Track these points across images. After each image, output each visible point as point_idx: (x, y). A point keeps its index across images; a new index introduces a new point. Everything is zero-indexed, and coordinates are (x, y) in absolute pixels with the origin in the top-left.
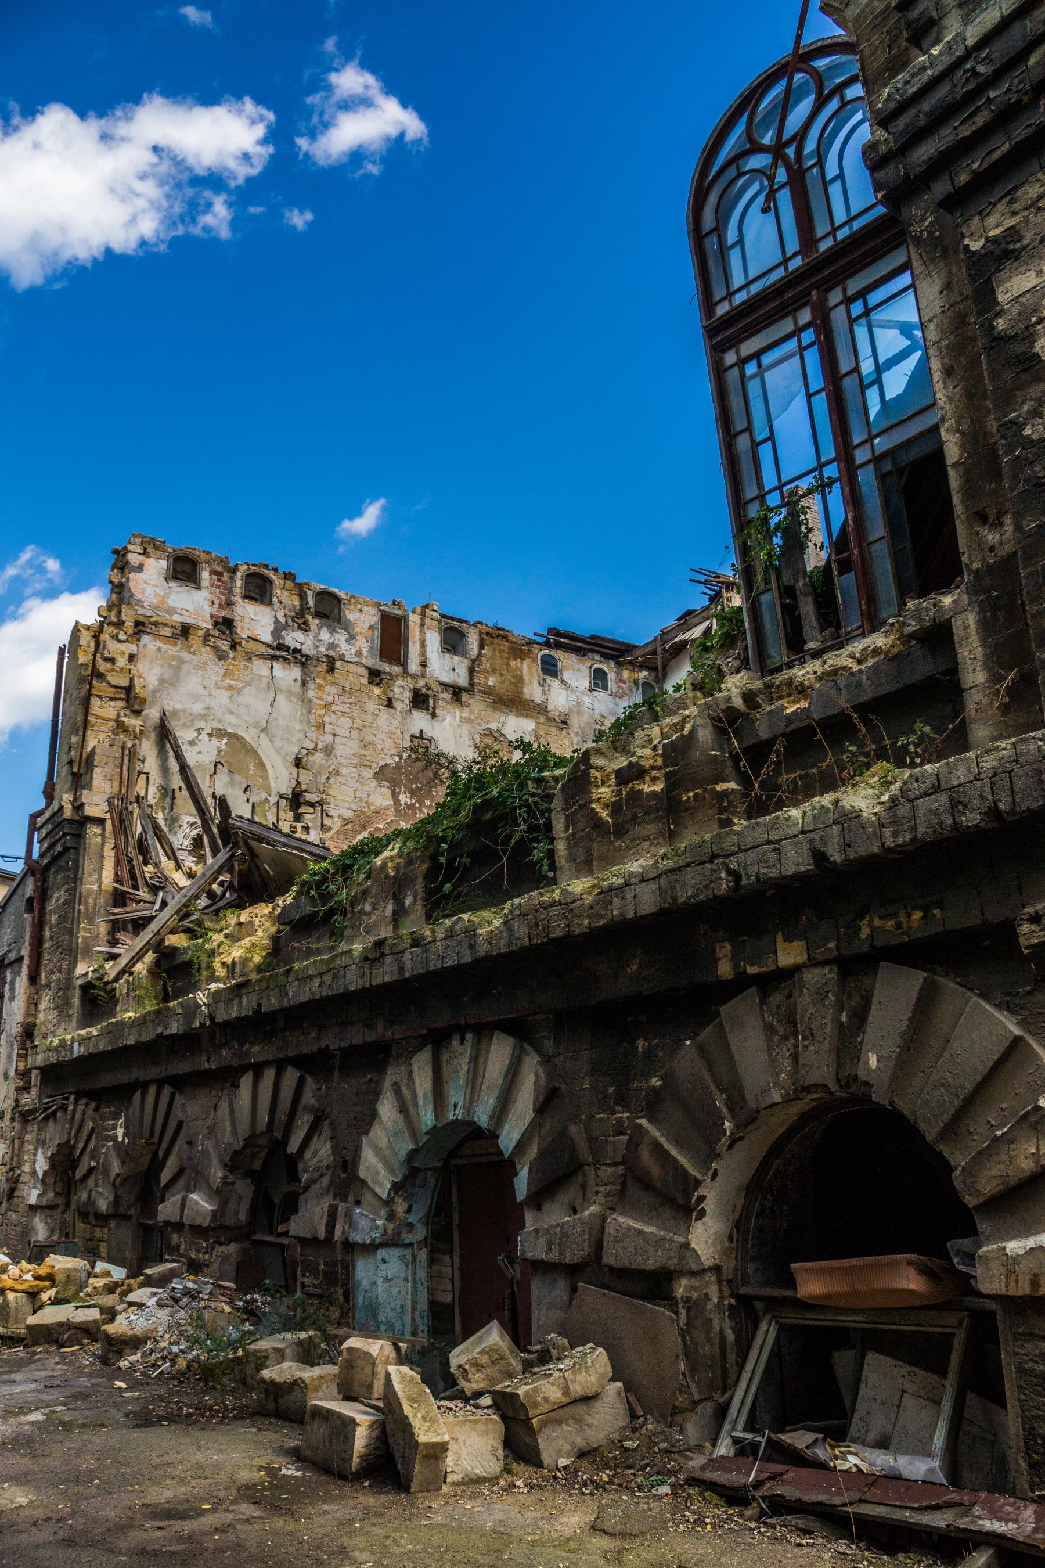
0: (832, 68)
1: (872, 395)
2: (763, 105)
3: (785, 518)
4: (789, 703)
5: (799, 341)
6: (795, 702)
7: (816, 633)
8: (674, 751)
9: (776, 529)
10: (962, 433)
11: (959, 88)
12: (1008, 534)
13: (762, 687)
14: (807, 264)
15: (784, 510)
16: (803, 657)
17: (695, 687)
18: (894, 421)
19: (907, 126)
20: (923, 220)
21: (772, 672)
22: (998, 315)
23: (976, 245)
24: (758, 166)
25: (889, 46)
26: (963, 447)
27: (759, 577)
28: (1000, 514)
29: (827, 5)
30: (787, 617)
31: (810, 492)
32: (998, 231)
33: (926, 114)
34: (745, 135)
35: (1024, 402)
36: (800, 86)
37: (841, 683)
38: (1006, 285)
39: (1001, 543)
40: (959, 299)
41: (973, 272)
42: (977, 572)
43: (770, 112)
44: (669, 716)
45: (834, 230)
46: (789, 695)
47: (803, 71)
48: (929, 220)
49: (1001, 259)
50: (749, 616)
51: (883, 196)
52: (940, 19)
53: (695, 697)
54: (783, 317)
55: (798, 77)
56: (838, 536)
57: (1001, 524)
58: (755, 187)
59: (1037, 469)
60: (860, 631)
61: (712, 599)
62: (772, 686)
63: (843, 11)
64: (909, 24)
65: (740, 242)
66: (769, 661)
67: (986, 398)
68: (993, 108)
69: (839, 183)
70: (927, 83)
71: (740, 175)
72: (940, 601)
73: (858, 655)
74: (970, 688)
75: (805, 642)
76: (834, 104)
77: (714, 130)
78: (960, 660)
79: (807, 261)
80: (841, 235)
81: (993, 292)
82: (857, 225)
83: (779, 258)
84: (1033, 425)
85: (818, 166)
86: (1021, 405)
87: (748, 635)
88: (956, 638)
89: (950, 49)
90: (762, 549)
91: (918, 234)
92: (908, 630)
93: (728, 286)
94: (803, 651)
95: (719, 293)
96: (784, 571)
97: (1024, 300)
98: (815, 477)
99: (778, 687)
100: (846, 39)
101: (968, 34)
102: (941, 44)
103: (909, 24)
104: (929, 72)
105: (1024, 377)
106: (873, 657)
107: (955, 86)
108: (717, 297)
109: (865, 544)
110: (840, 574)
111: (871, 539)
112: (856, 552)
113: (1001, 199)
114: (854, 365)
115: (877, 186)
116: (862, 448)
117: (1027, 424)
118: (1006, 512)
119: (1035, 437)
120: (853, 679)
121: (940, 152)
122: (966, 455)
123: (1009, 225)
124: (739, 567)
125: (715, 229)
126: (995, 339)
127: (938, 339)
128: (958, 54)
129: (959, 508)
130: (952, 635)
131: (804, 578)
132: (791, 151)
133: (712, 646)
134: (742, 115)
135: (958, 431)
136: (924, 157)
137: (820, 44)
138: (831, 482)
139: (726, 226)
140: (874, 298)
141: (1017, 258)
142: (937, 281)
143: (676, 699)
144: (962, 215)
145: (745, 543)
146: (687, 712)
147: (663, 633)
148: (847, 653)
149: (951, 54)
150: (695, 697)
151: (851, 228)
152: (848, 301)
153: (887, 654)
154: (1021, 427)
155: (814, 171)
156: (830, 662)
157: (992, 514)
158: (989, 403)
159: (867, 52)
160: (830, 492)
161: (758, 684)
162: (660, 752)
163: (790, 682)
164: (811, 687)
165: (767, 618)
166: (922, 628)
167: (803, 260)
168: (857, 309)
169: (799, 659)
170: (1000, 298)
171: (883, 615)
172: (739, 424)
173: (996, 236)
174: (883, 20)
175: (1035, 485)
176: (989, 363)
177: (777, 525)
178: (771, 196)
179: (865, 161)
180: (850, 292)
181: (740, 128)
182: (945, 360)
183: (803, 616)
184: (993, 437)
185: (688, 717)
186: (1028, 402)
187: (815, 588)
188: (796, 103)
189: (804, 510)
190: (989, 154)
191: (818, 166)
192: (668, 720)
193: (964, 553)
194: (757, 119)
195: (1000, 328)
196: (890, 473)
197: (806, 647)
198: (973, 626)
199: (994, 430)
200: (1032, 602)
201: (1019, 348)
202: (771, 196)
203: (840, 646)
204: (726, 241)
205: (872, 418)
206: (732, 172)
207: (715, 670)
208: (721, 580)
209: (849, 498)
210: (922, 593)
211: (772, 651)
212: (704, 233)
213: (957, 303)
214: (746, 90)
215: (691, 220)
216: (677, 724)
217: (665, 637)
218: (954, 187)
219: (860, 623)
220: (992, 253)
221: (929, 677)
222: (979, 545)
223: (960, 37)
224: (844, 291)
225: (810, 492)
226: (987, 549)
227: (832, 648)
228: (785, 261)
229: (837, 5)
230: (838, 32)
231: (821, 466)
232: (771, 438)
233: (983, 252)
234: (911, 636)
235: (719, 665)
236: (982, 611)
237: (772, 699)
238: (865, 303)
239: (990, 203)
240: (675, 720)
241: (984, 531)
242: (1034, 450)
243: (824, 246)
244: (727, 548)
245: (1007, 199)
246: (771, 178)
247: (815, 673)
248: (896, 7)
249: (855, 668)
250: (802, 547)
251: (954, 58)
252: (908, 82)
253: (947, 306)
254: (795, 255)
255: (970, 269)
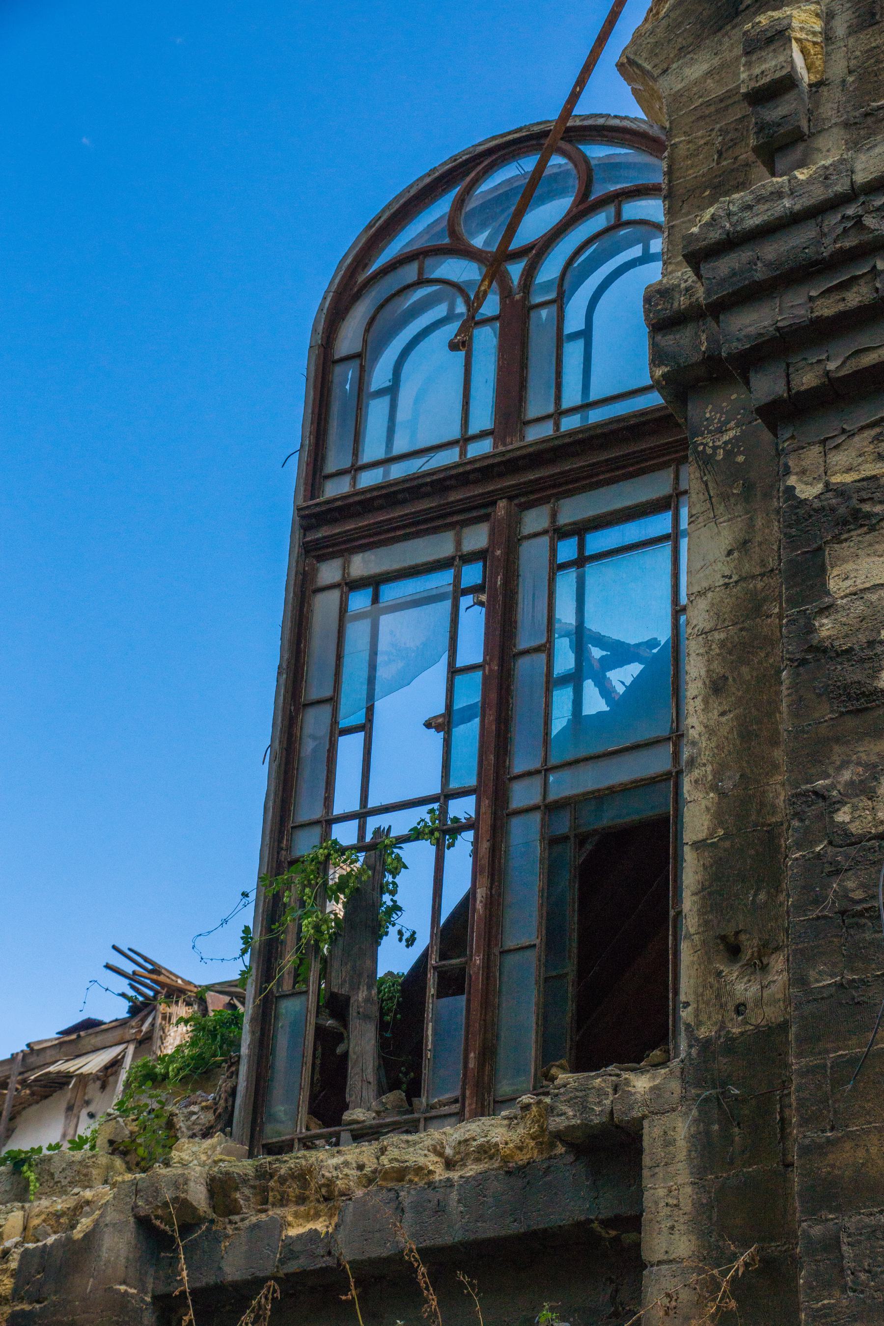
0: (612, 167)
1: (562, 699)
2: (486, 186)
3: (361, 871)
4: (296, 1215)
5: (457, 578)
6: (308, 1217)
7: (369, 1093)
8: (43, 1269)
9: (342, 885)
10: (722, 794)
11: (827, 241)
12: (773, 988)
13: (251, 1172)
14: (503, 454)
15: (362, 856)
16: (337, 1135)
17: (115, 1147)
18: (582, 753)
19: (734, 273)
20: (721, 431)
21: (278, 1149)
22: (825, 610)
23: (807, 491)
24: (454, 278)
25: (720, 153)
26: (719, 817)
27: (289, 960)
28: (767, 948)
29: (631, 62)
30: (320, 1050)
31: (416, 835)
32: (848, 478)
33: (769, 265)
34: (444, 223)
35: (845, 764)
36: (555, 177)
37: (407, 1198)
38: (849, 566)
39: (759, 1002)
40: (757, 571)
41: (793, 531)
42: (706, 1045)
43: (499, 199)
44: (47, 1195)
45: (559, 414)
46: (302, 1200)
47: (564, 153)
48: (731, 434)
49: (845, 523)
50: (253, 1033)
51: (663, 375)
52: (812, 135)
53: (110, 1167)
54: (435, 530)
55: (557, 161)
56: (448, 921)
57: (764, 968)
58: (440, 311)
59: (850, 884)
60: (455, 1108)
61: (135, 1010)
62: (272, 1176)
63: (655, 80)
64: (761, 127)
65: (392, 391)
66: (269, 1129)
67: (774, 742)
68: (878, 285)
69: (580, 344)
70: (780, 218)
71: (422, 282)
72: (627, 1082)
73: (449, 1151)
74: (660, 1263)
75: (346, 1107)
76: (599, 221)
77: (396, 198)
78: (647, 1202)
79: (501, 448)
80: (570, 423)
81: (822, 571)
82: (596, 416)
83: (455, 432)
84: (855, 808)
85: (554, 308)
86: (839, 769)
87: (243, 1069)
88: (646, 1160)
89: (826, 178)
90: (307, 915)
91: (709, 451)
92: (557, 1123)
93: (356, 453)
94: (338, 1122)
95: (335, 460)
96: (336, 964)
97: (874, 597)
98: (431, 811)
99: (282, 1180)
100: (644, 127)
101: (858, 166)
102: (814, 168)
103: (761, 127)
104: (787, 203)
105: (851, 722)
106: (478, 1160)
107: (824, 235)
108: (331, 467)
109: (496, 951)
110: (440, 994)
111: (510, 944)
112: (478, 960)
113: (862, 429)
114: (543, 640)
115: (658, 357)
116: (525, 782)
117: (844, 804)
118: (777, 949)
119: (855, 828)
120: (430, 1194)
121: (778, 329)
122: (721, 832)
123: (869, 473)
124: (257, 938)
125: (358, 356)
126: (811, 649)
127: (708, 626)
128: (839, 188)
129: (691, 923)
130: (640, 1151)
131: (370, 987)
132: (515, 270)
133: (165, 1076)
134: (445, 191)
135: (714, 788)
136: (752, 330)
137: (601, 121)
138: (456, 829)
139: (375, 359)
140: (597, 542)
141: (872, 529)
142: (725, 533)
143: (71, 1164)
144: (793, 437)
145: (277, 897)
146: (88, 1194)
147: (32, 1050)
148: (428, 1142)
149: (827, 187)
150: (110, 1167)
151: (585, 418)
152: (559, 533)
153: (505, 1160)
154: (834, 806)
155: (544, 313)
156: (393, 1152)
157: (750, 946)
158: (779, 754)
159: (682, 150)
160: (452, 845)
161: (245, 1167)
162: (14, 1265)
163: (302, 1176)
164: (346, 1194)
165: (282, 1042)
166: (585, 1126)
167: (495, 446)
168: (567, 550)
169: (327, 1138)
170: (832, 585)
171: (504, 1088)
172: (319, 687)
173: (844, 484)
174: (717, 111)
175: (843, 913)
176: (794, 686)
177: (344, 881)
178: (472, 322)
179: (647, 312)
180: (564, 518)
181: (442, 207)
182: (715, 665)
183: (352, 1056)
184: (774, 814)
185: (88, 1203)
186: (851, 767)
187: (382, 1013)
188: (543, 200)
189: (399, 866)
190: (858, 352)
191: (554, 308)
192: (45, 1202)
193: (687, 1004)
194: (472, 204)
195: (824, 633)
196: (565, 838)
197: (347, 1116)
198: (682, 1144)
199: (780, 801)
200: (805, 1122)
201: (853, 674)
202: (472, 322)
203: (412, 1128)
204: (369, 384)
205: (555, 731)
206: (410, 272)
207: (163, 1120)
208: (162, 978)
209: (485, 862)
210: (578, 1067)
211: (280, 1109)
212: (336, 357)
213: (753, 577)
214: (464, 153)
215: (320, 329)
216: (63, 1214)
217: (32, 1059)
218: (789, 390)
219: (457, 1093)
220: (833, 510)
221: (579, 1224)
222: (718, 997)
223: (845, 167)
224: (554, 516)
225: (416, 835)
226: (731, 1007)
227: (395, 1127)
228: (465, 440)
229: (648, 67)
230: (637, 112)
231: (447, 795)
232: (366, 727)
233: (817, 504)
234: (558, 1136)
235: (172, 1115)
236: (703, 1119)
237: (265, 1201)
238: (581, 546)
239: (844, 431)
240: (61, 1204)
241: (732, 973)
242: (852, 851)
243: (535, 434)
244: (245, 895)
245: (874, 432)
246: (473, 306)
247: (361, 1167)
248: (747, 96)
249: (440, 1174)
250: (377, 933)
251: (830, 193)
252: (749, 207)
253: (735, 578)
254: (483, 435)
255: (790, 526)
